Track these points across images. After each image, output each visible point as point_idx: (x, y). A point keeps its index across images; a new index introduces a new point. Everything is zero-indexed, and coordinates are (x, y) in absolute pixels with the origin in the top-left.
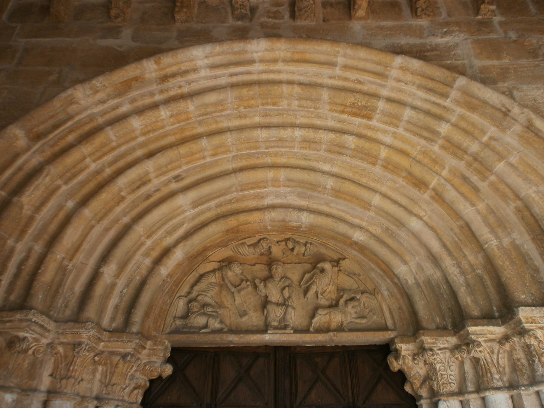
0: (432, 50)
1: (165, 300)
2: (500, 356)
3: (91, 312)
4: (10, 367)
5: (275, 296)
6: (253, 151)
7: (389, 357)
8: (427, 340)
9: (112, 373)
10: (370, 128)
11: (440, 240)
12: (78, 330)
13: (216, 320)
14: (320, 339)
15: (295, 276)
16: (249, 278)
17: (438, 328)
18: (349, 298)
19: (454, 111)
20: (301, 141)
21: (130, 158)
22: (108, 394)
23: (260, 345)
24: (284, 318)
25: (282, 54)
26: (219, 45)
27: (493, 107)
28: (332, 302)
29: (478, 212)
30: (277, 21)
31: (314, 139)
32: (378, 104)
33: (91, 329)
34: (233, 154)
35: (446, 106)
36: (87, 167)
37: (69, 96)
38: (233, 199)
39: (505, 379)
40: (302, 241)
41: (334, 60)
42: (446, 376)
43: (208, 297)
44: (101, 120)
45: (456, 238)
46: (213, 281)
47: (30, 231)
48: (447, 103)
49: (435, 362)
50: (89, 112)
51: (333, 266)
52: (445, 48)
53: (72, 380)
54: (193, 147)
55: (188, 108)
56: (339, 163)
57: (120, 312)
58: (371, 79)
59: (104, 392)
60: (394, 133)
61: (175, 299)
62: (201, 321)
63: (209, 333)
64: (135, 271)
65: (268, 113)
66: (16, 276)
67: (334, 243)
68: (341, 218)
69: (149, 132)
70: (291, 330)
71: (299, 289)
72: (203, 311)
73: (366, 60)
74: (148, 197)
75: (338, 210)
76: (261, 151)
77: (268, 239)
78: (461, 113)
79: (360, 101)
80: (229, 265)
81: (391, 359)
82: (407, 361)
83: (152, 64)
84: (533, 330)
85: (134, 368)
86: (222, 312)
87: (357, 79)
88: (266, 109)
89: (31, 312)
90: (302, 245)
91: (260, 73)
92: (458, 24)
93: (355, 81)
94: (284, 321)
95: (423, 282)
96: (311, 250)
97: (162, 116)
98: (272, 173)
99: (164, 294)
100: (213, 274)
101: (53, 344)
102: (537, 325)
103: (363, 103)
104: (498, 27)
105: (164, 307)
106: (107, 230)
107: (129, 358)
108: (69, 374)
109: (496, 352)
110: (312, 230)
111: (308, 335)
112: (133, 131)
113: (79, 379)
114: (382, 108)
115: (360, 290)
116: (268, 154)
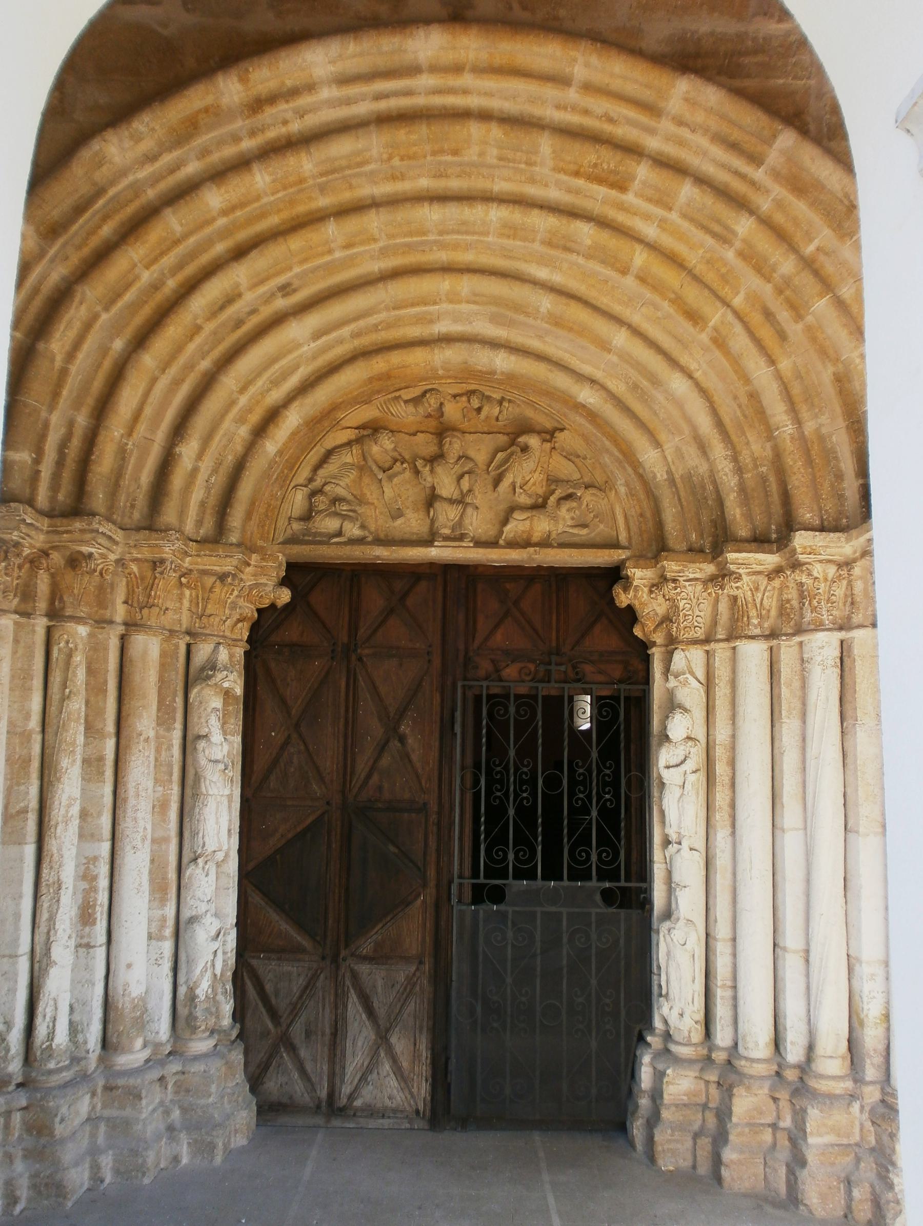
0: (756, 52)
2: (766, 594)
3: (169, 515)
4: (76, 591)
5: (447, 488)
6: (415, 239)
7: (615, 586)
8: (671, 567)
9: (206, 600)
10: (622, 207)
11: (714, 412)
12: (157, 542)
13: (355, 524)
14: (515, 556)
15: (480, 455)
16: (407, 457)
17: (690, 550)
18: (564, 494)
21: (205, 259)
22: (204, 628)
24: (460, 523)
26: (355, 38)
28: (537, 500)
33: (176, 541)
34: (381, 244)
35: (756, 179)
39: (766, 625)
40: (494, 396)
42: (691, 617)
44: (151, 194)
45: (739, 413)
46: (348, 461)
47: (65, 393)
48: (759, 174)
49: (679, 598)
50: (131, 178)
51: (544, 440)
53: (155, 610)
55: (302, 167)
56: (565, 266)
57: (209, 511)
58: (631, 113)
59: (197, 625)
61: (290, 488)
62: (332, 524)
63: (345, 543)
64: (225, 447)
66: (60, 463)
67: (548, 402)
70: (471, 541)
71: (486, 476)
72: (333, 509)
74: (239, 323)
77: (439, 392)
80: (373, 435)
81: (618, 590)
84: (809, 563)
85: (236, 593)
86: (363, 510)
87: (606, 114)
88: (440, 163)
90: (495, 403)
93: (601, 117)
94: (460, 527)
95: (682, 476)
96: (509, 411)
98: (447, 283)
100: (347, 449)
101: (124, 561)
105: (272, 502)
107: (229, 580)
108: (151, 601)
109: (762, 588)
110: (511, 379)
111: (496, 550)
113: (164, 608)
114: (643, 178)
115: (584, 483)
116: (443, 246)
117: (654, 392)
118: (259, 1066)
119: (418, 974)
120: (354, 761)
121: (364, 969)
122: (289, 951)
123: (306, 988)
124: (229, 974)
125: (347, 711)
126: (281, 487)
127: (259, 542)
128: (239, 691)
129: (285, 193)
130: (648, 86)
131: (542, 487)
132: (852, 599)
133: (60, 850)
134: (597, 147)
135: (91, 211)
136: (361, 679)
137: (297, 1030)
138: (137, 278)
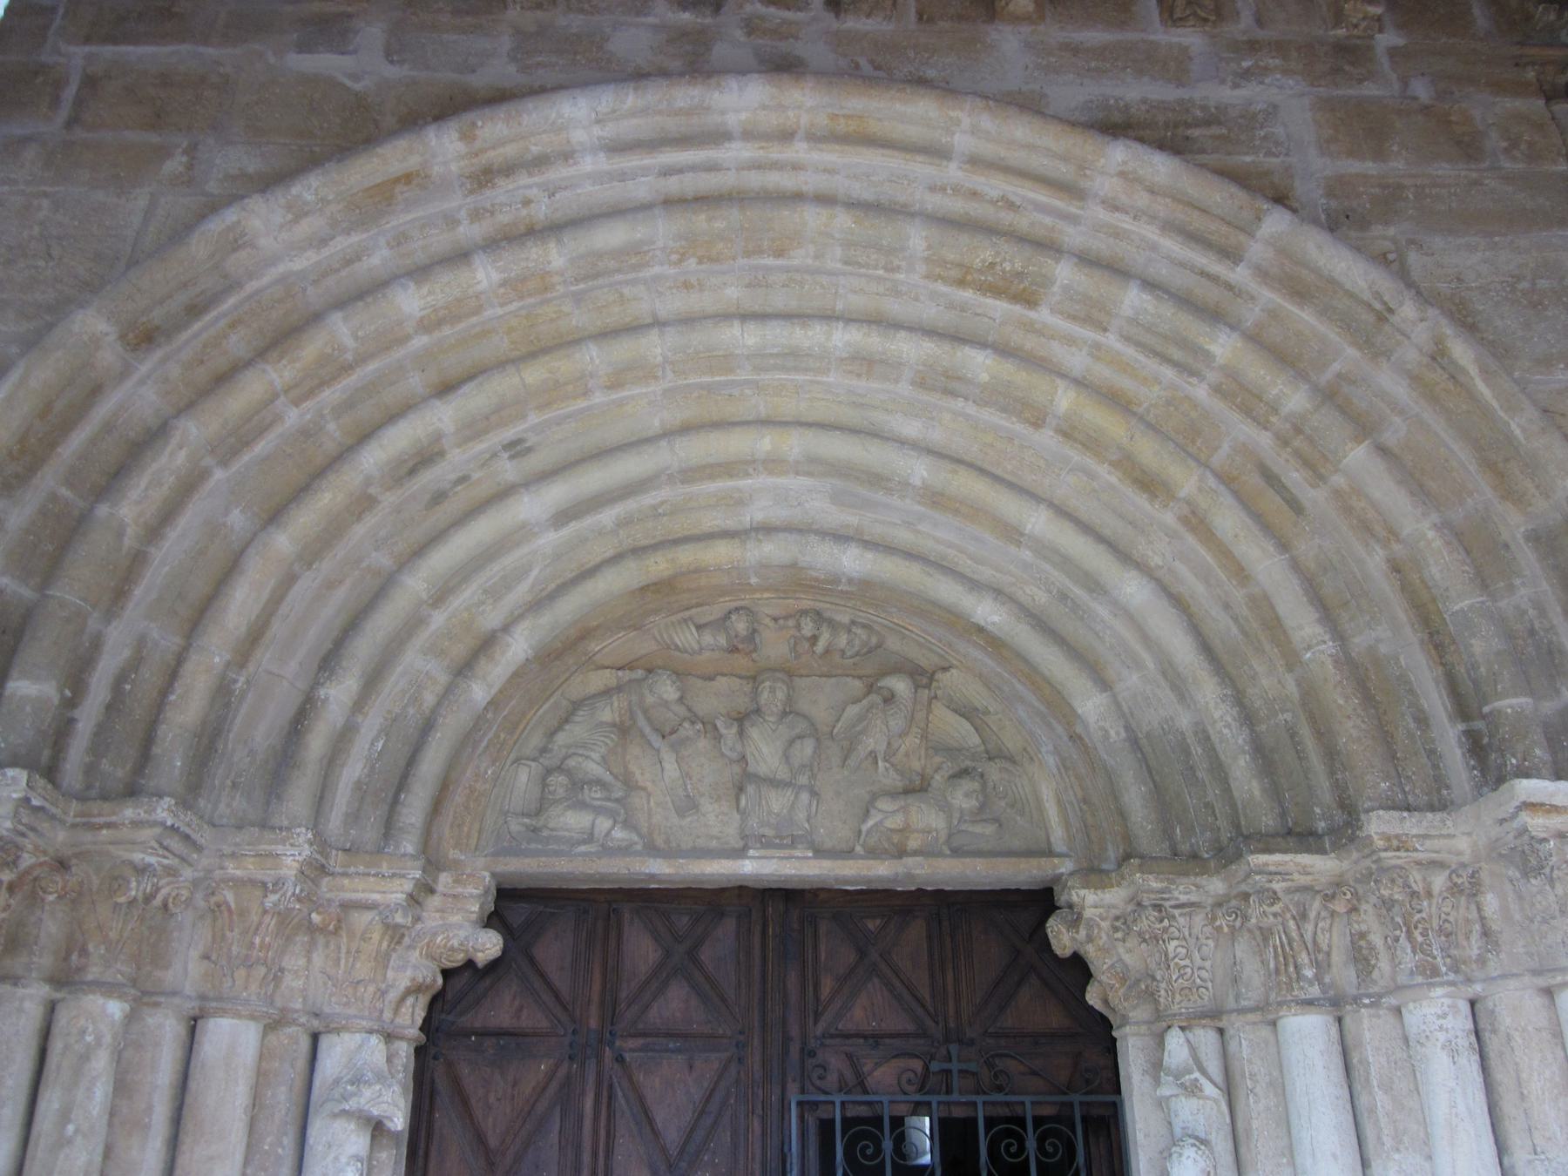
0: (1208, 123)
1: (482, 770)
2: (1320, 925)
6: (717, 378)
10: (1029, 327)
14: (881, 871)
19: (1252, 298)
23: (724, 886)
27: (1351, 295)
32: (1057, 272)
37: (230, 229)
38: (662, 503)
41: (944, 141)
43: (593, 760)
48: (1240, 275)
49: (1165, 937)
50: (281, 268)
52: (1242, 117)
54: (559, 368)
58: (1042, 196)
60: (1097, 346)
61: (509, 763)
65: (761, 278)
68: (944, 563)
69: (440, 323)
73: (1031, 147)
74: (439, 497)
76: (738, 378)
79: (1008, 258)
82: (1096, 931)
83: (452, 142)
87: (1003, 197)
89: (162, 802)
91: (743, 169)
92: (1280, 48)
93: (998, 201)
97: (479, 283)
99: (479, 752)
102: (1410, 854)
103: (1018, 266)
104: (1385, 62)
105: (478, 786)
106: (330, 585)
109: (1312, 915)
110: (865, 589)
111: (851, 862)
117: (1095, 605)
125: (595, 1154)
126: (494, 762)
127: (451, 851)
128: (399, 1121)
129: (521, 304)
130: (1065, 158)
131: (919, 759)
132: (1483, 925)
134: (994, 240)
135: (213, 314)
136: (620, 1094)
138: (278, 418)
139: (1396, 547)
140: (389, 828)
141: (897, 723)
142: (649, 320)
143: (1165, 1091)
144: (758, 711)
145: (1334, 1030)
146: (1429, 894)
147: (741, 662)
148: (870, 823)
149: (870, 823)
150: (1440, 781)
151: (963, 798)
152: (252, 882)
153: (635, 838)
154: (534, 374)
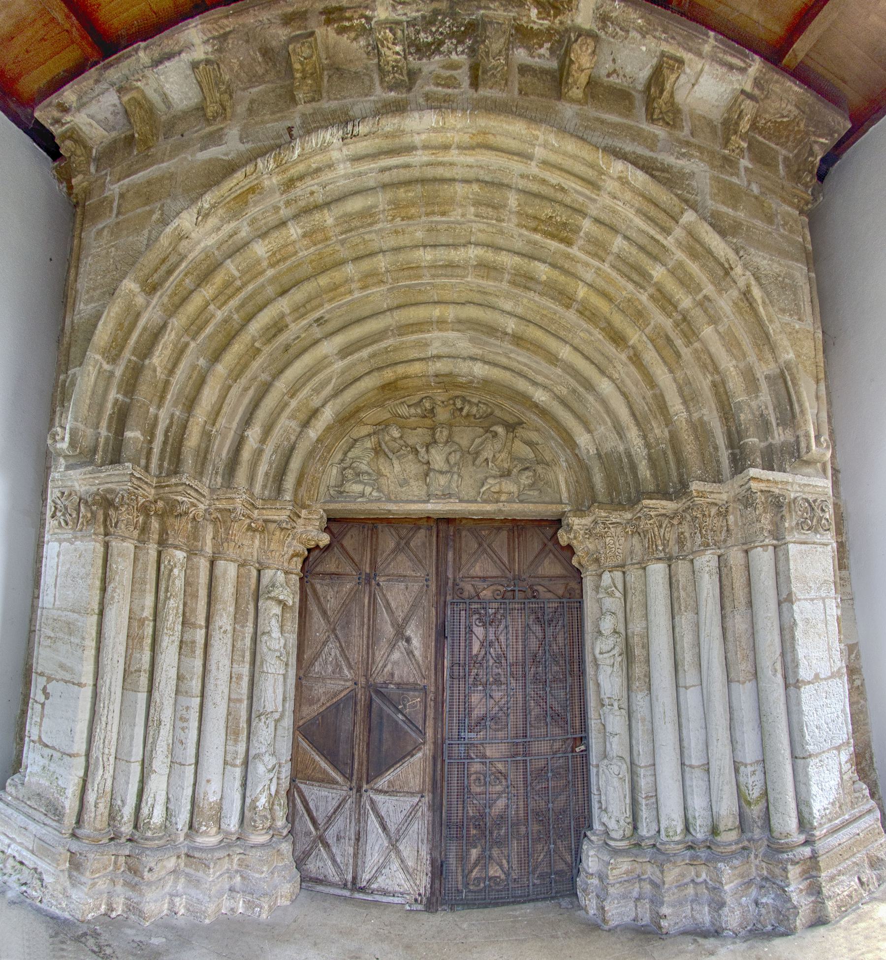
4: (176, 528)
10: (568, 256)
20: (477, 265)
25: (455, 137)
27: (716, 259)
29: (675, 380)
30: (450, 91)
31: (494, 262)
34: (389, 286)
36: (213, 316)
58: (578, 186)
60: (599, 269)
66: (165, 443)
74: (287, 348)
75: (518, 362)
78: (680, 259)
81: (561, 532)
88: (432, 222)
98: (437, 310)
103: (564, 219)
106: (246, 389)
112: (258, 262)
117: (587, 396)
118: (303, 853)
119: (420, 804)
120: (373, 654)
121: (379, 798)
122: (326, 781)
123: (338, 807)
124: (283, 793)
125: (369, 620)
133: (161, 697)
137: (330, 835)
139: (716, 376)
140: (279, 490)
141: (498, 446)
142: (378, 250)
143: (601, 596)
144: (435, 442)
145: (667, 570)
146: (710, 516)
147: (428, 422)
148: (484, 488)
149: (484, 488)
150: (719, 472)
151: (525, 479)
152: (226, 510)
153: (382, 495)
154: (323, 281)
